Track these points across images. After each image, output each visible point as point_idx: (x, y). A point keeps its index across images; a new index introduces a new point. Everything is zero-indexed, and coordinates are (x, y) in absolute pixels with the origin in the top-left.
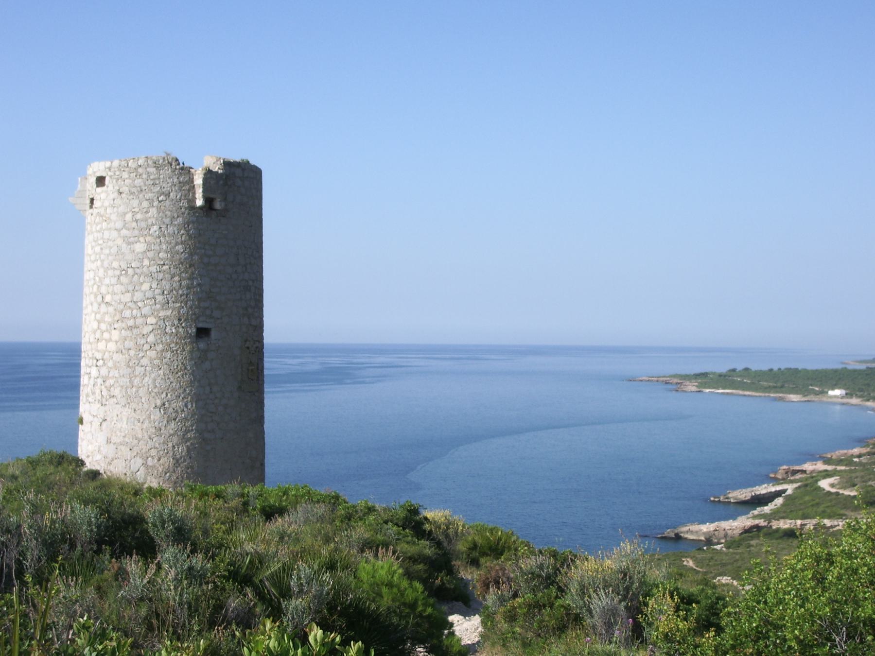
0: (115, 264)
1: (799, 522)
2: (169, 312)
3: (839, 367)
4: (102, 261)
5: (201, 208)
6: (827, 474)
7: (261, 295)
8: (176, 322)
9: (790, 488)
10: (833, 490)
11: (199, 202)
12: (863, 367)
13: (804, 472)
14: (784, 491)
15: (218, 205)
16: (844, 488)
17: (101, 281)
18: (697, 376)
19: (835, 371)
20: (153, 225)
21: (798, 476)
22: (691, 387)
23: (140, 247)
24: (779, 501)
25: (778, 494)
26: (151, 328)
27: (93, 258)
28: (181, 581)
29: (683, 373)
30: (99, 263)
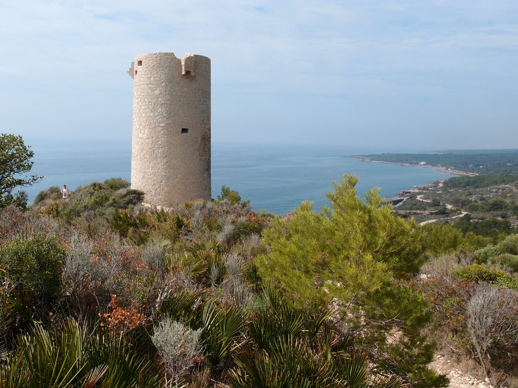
0: (146, 100)
1: (408, 211)
2: (170, 122)
3: (424, 153)
4: (141, 98)
5: (184, 75)
6: (419, 194)
7: (210, 121)
8: (173, 126)
9: (405, 199)
10: (421, 200)
11: (183, 73)
12: (433, 153)
13: (410, 193)
14: (403, 200)
15: (192, 74)
16: (425, 199)
17: (140, 108)
18: (370, 156)
19: (422, 155)
20: (163, 83)
21: (407, 194)
22: (367, 160)
23: (157, 92)
24: (401, 203)
25: (400, 201)
26: (162, 128)
27: (137, 97)
28: (110, 308)
29: (365, 154)
30: (139, 99)
